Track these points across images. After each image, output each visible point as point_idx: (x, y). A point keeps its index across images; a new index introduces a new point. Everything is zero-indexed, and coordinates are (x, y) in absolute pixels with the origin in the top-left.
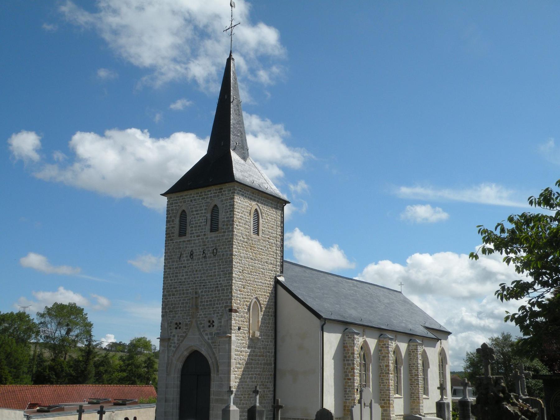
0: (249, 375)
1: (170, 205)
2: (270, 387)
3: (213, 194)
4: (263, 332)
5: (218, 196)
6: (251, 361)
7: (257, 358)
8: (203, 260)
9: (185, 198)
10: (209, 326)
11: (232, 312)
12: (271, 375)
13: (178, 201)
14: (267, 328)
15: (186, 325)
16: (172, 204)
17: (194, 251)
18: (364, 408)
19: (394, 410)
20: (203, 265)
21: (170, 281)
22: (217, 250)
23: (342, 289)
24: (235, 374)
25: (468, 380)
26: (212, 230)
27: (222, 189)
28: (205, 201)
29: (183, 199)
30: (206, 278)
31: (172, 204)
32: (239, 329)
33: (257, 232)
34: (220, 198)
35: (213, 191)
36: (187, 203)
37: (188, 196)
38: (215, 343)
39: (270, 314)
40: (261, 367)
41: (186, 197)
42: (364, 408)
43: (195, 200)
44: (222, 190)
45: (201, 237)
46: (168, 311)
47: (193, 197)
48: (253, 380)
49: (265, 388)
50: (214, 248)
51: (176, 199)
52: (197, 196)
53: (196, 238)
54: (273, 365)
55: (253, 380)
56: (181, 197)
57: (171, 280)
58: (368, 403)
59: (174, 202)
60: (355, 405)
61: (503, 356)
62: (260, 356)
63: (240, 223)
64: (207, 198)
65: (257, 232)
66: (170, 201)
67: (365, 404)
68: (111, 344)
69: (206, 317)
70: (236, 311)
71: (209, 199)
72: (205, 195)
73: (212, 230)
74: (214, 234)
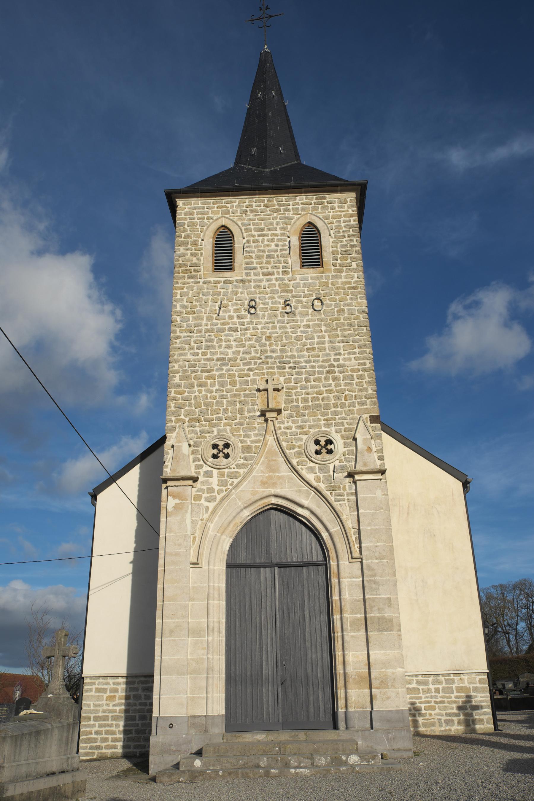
3: (301, 206)
8: (286, 318)
10: (318, 452)
15: (247, 449)
17: (257, 300)
20: (282, 271)
21: (189, 357)
23: (270, 56)
26: (304, 264)
30: (296, 354)
38: (339, 488)
45: (276, 276)
46: (187, 419)
50: (314, 297)
53: (261, 277)
61: (265, 47)
68: (103, 280)
69: (305, 433)
71: (292, 213)
73: (304, 264)
74: (310, 273)
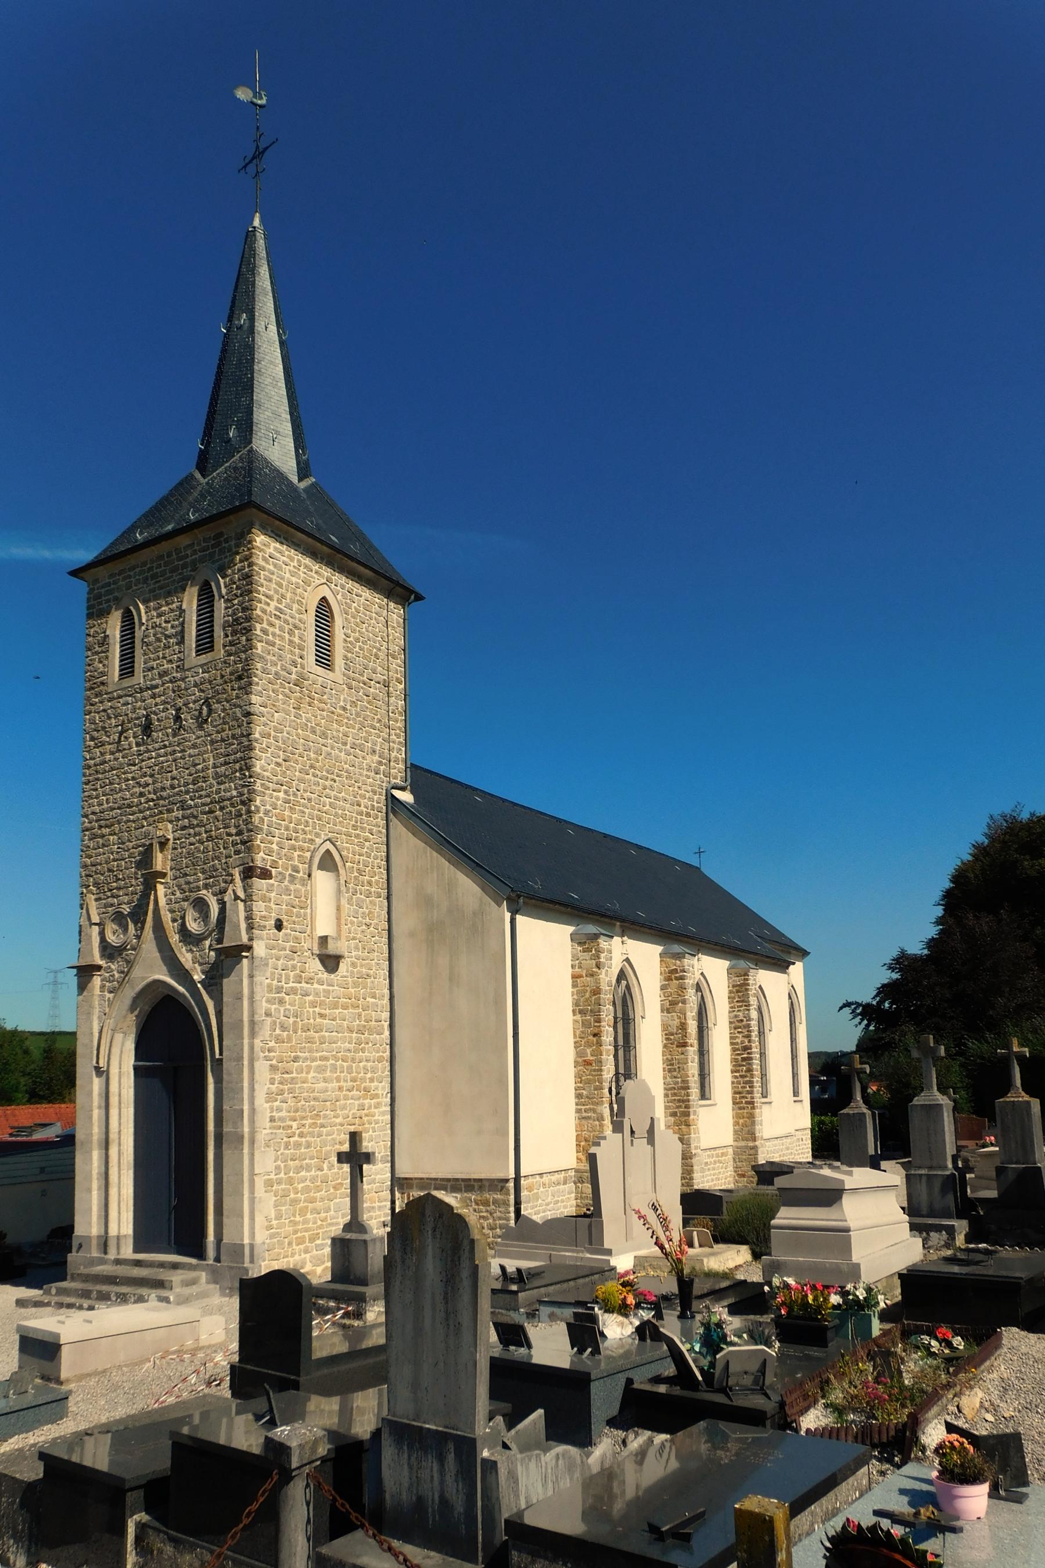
0: (314, 1060)
1: (94, 600)
2: (380, 1092)
3: (200, 554)
4: (354, 939)
5: (212, 555)
6: (318, 1020)
7: (337, 1011)
9: (130, 577)
11: (251, 877)
12: (380, 1060)
13: (112, 586)
14: (364, 927)
16: (99, 596)
18: (632, 1145)
19: (699, 1138)
22: (209, 706)
24: (267, 1059)
25: (776, 1338)
27: (221, 534)
28: (180, 574)
29: (124, 579)
31: (99, 596)
32: (279, 925)
33: (324, 659)
34: (217, 561)
35: (199, 544)
36: (135, 588)
37: (137, 570)
39: (373, 889)
40: (351, 1037)
41: (132, 573)
42: (632, 1145)
43: (153, 577)
44: (222, 539)
47: (150, 569)
48: (328, 1074)
49: (365, 1097)
51: (107, 581)
52: (160, 566)
54: (387, 1033)
55: (328, 1074)
56: (119, 575)
57: (100, 804)
58: (642, 1129)
59: (103, 590)
60: (604, 1138)
62: (345, 1007)
63: (272, 625)
64: (184, 566)
65: (324, 659)
66: (94, 589)
67: (632, 1132)
70: (266, 874)
72: (180, 559)
